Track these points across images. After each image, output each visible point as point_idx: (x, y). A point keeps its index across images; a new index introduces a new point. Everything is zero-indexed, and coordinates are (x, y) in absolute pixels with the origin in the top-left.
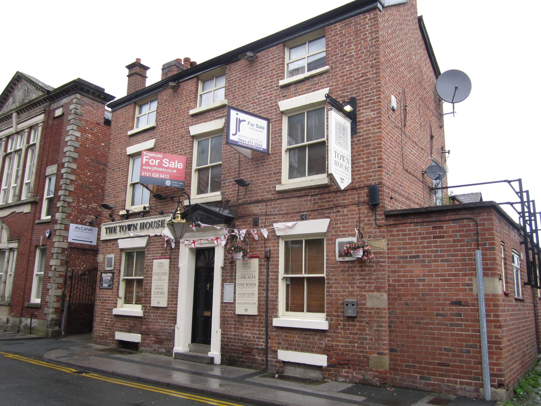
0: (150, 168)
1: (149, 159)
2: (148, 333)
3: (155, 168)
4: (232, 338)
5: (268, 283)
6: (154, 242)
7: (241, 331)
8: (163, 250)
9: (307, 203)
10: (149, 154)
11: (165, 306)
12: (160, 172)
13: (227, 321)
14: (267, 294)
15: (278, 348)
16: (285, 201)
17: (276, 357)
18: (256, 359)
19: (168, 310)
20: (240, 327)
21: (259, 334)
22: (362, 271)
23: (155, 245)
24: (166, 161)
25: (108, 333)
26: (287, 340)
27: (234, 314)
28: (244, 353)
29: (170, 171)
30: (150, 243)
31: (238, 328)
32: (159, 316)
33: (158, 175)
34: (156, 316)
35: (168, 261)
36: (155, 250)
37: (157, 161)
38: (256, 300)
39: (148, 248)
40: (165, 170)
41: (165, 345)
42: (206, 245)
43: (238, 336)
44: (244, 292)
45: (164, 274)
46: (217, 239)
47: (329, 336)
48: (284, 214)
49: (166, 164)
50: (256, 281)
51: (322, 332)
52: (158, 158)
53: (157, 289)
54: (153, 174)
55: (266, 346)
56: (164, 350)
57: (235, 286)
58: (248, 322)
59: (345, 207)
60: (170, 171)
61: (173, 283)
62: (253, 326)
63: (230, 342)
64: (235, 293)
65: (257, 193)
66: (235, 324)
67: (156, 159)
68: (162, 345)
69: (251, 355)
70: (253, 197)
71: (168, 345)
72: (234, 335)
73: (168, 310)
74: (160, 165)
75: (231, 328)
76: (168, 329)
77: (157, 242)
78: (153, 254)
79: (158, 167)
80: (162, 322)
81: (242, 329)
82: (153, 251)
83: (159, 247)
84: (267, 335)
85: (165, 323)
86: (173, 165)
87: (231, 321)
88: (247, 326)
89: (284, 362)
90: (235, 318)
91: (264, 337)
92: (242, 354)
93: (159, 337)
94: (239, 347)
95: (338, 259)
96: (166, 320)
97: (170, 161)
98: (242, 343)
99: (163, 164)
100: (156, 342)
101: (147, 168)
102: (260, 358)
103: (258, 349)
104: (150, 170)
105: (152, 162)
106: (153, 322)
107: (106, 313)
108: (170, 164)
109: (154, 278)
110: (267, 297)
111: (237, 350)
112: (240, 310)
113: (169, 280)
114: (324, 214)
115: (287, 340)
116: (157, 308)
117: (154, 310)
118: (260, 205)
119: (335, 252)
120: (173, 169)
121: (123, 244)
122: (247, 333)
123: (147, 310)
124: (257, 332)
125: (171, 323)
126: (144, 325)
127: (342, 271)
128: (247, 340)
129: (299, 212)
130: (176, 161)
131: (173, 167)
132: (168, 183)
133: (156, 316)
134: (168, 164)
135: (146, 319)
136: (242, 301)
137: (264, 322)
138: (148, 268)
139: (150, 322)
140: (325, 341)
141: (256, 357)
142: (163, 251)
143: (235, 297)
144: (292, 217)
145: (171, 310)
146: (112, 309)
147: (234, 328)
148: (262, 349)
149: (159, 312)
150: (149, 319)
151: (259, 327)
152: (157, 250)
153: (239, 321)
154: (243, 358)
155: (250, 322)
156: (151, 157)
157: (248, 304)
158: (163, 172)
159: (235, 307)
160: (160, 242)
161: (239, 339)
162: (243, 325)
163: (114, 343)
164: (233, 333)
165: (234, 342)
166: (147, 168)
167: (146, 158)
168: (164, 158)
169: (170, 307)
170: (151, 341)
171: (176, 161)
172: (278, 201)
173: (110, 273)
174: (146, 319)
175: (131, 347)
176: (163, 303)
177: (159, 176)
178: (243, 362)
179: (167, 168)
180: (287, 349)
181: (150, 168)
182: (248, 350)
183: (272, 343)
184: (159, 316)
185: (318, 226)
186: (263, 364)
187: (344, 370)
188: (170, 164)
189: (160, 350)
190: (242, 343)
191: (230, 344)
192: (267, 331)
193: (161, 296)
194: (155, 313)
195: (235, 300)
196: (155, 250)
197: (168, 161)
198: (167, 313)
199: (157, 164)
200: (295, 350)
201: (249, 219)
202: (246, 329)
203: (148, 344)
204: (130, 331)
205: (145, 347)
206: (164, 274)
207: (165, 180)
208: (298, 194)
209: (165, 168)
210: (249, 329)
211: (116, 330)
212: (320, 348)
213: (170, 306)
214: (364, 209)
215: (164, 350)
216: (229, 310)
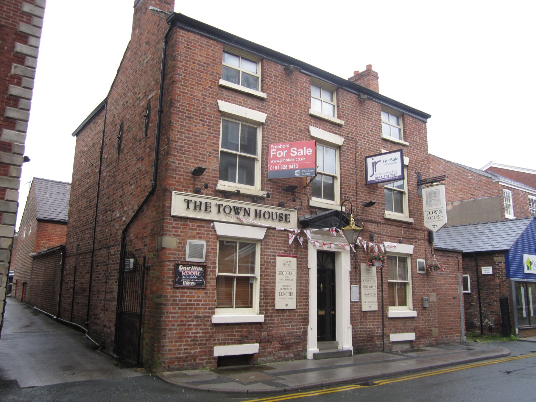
0: (278, 161)
1: (276, 152)
2: (271, 340)
3: (283, 160)
4: (358, 331)
5: (382, 286)
6: (274, 236)
7: (365, 324)
8: (287, 247)
9: (402, 232)
10: (276, 147)
11: (295, 307)
12: (288, 163)
13: (355, 317)
14: (382, 294)
15: (390, 333)
16: (389, 226)
17: (389, 340)
18: (376, 344)
19: (297, 312)
20: (365, 321)
21: (378, 325)
22: (428, 280)
23: (276, 239)
24: (294, 150)
25: (199, 350)
26: (395, 327)
27: (361, 310)
28: (368, 341)
29: (299, 159)
30: (268, 236)
31: (363, 322)
32: (285, 319)
33: (286, 166)
34: (282, 319)
35: (294, 260)
36: (276, 246)
37: (285, 152)
38: (376, 299)
39: (266, 242)
40: (293, 160)
41: (293, 349)
42: (332, 248)
43: (363, 328)
44: (368, 293)
45: (291, 273)
46: (340, 244)
47: (416, 321)
48: (389, 236)
49: (294, 153)
50: (375, 284)
51: (412, 318)
52: (286, 149)
53: (284, 289)
54: (281, 167)
55: (383, 333)
56: (292, 355)
57: (360, 288)
58: (370, 316)
59: (419, 240)
60: (299, 159)
61: (300, 283)
62: (374, 319)
63: (357, 334)
64: (360, 293)
65: (371, 214)
66: (361, 319)
67: (283, 150)
68: (289, 349)
69: (373, 342)
70: (368, 217)
71: (297, 348)
72: (361, 328)
73: (297, 312)
74: (288, 155)
75: (357, 323)
76: (296, 332)
77: (277, 236)
78: (274, 249)
79: (286, 158)
80: (289, 326)
81: (366, 322)
82: (273, 246)
83: (281, 243)
84: (383, 324)
85: (292, 326)
86: (301, 152)
87: (357, 317)
88: (370, 319)
89: (393, 342)
90: (361, 314)
91: (381, 326)
92: (367, 342)
93: (284, 342)
94: (364, 337)
95: (419, 272)
96: (294, 322)
97: (298, 149)
98: (366, 334)
99: (291, 154)
100: (281, 349)
101: (275, 161)
102: (379, 343)
103: (377, 336)
104: (279, 163)
105: (280, 154)
106: (278, 327)
107: (194, 323)
108: (297, 152)
109: (278, 277)
110: (382, 296)
111: (363, 340)
112: (365, 308)
113: (297, 280)
114: (410, 242)
115: (395, 327)
116: (283, 311)
117: (278, 313)
118: (373, 224)
119: (416, 267)
120: (301, 157)
121: (222, 230)
122: (370, 325)
123: (268, 314)
124: (377, 324)
125: (300, 325)
126: (265, 331)
127: (420, 280)
128: (370, 331)
129: (397, 237)
130: (305, 148)
131: (302, 154)
132: (297, 174)
133: (282, 319)
134: (296, 152)
135: (268, 324)
136: (366, 300)
137: (381, 315)
138: (267, 265)
139: (273, 327)
140: (414, 324)
141: (377, 343)
142: (286, 249)
143: (360, 296)
144: (393, 239)
145: (300, 312)
146: (210, 317)
147: (360, 322)
148: (380, 336)
149: (285, 314)
150: (272, 323)
151: (378, 319)
152: (279, 246)
153: (363, 317)
154: (367, 345)
155: (371, 316)
156: (278, 150)
157: (370, 304)
158: (291, 163)
159: (361, 305)
160: (281, 237)
161: (364, 331)
162: (366, 319)
163: (211, 363)
164: (360, 327)
165: (360, 334)
166: (275, 161)
167: (273, 152)
168: (291, 146)
169: (299, 309)
170: (275, 348)
171: (305, 148)
172: (385, 226)
173: (198, 266)
174: (268, 324)
175: (245, 360)
176: (292, 304)
177: (288, 167)
178: (368, 349)
179: (295, 157)
180: (395, 332)
181: (278, 161)
182: (371, 338)
183: (386, 330)
184: (285, 319)
185: (407, 249)
186: (381, 347)
187: (422, 340)
188: (297, 152)
189: (287, 356)
190: (366, 334)
191: (357, 336)
192: (383, 322)
193: (289, 297)
194: (280, 316)
195: (360, 299)
196: (276, 246)
197: (296, 149)
198: (295, 316)
199: (284, 156)
200: (400, 332)
201: (366, 234)
202: (369, 322)
203: (270, 353)
204: (240, 342)
205: (265, 356)
206: (291, 273)
207: (293, 170)
208: (396, 224)
209: (293, 157)
210: (371, 322)
211: (215, 344)
212: (411, 329)
213: (299, 307)
214: (427, 242)
215: (292, 355)
216: (356, 308)
